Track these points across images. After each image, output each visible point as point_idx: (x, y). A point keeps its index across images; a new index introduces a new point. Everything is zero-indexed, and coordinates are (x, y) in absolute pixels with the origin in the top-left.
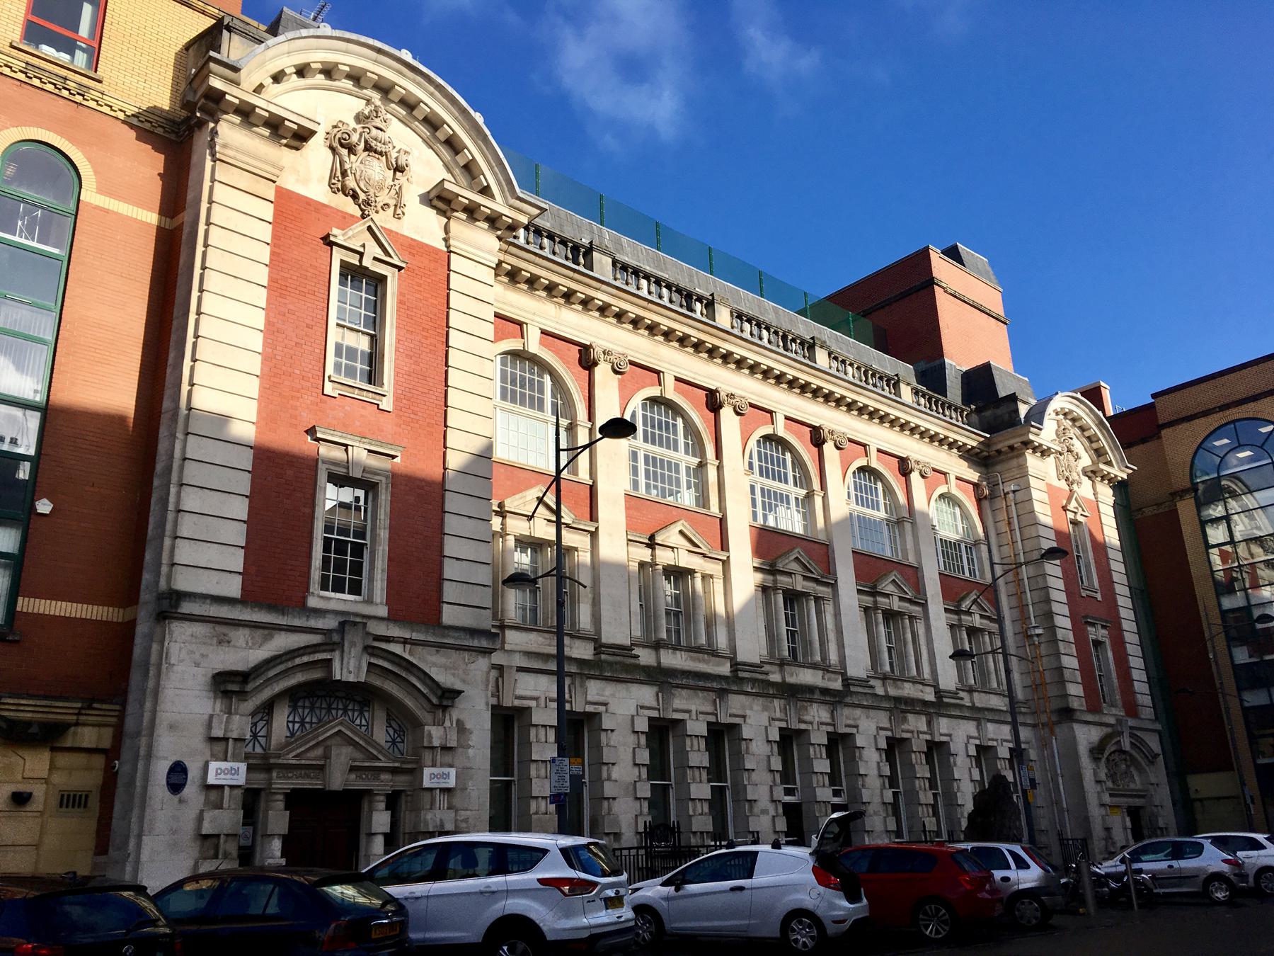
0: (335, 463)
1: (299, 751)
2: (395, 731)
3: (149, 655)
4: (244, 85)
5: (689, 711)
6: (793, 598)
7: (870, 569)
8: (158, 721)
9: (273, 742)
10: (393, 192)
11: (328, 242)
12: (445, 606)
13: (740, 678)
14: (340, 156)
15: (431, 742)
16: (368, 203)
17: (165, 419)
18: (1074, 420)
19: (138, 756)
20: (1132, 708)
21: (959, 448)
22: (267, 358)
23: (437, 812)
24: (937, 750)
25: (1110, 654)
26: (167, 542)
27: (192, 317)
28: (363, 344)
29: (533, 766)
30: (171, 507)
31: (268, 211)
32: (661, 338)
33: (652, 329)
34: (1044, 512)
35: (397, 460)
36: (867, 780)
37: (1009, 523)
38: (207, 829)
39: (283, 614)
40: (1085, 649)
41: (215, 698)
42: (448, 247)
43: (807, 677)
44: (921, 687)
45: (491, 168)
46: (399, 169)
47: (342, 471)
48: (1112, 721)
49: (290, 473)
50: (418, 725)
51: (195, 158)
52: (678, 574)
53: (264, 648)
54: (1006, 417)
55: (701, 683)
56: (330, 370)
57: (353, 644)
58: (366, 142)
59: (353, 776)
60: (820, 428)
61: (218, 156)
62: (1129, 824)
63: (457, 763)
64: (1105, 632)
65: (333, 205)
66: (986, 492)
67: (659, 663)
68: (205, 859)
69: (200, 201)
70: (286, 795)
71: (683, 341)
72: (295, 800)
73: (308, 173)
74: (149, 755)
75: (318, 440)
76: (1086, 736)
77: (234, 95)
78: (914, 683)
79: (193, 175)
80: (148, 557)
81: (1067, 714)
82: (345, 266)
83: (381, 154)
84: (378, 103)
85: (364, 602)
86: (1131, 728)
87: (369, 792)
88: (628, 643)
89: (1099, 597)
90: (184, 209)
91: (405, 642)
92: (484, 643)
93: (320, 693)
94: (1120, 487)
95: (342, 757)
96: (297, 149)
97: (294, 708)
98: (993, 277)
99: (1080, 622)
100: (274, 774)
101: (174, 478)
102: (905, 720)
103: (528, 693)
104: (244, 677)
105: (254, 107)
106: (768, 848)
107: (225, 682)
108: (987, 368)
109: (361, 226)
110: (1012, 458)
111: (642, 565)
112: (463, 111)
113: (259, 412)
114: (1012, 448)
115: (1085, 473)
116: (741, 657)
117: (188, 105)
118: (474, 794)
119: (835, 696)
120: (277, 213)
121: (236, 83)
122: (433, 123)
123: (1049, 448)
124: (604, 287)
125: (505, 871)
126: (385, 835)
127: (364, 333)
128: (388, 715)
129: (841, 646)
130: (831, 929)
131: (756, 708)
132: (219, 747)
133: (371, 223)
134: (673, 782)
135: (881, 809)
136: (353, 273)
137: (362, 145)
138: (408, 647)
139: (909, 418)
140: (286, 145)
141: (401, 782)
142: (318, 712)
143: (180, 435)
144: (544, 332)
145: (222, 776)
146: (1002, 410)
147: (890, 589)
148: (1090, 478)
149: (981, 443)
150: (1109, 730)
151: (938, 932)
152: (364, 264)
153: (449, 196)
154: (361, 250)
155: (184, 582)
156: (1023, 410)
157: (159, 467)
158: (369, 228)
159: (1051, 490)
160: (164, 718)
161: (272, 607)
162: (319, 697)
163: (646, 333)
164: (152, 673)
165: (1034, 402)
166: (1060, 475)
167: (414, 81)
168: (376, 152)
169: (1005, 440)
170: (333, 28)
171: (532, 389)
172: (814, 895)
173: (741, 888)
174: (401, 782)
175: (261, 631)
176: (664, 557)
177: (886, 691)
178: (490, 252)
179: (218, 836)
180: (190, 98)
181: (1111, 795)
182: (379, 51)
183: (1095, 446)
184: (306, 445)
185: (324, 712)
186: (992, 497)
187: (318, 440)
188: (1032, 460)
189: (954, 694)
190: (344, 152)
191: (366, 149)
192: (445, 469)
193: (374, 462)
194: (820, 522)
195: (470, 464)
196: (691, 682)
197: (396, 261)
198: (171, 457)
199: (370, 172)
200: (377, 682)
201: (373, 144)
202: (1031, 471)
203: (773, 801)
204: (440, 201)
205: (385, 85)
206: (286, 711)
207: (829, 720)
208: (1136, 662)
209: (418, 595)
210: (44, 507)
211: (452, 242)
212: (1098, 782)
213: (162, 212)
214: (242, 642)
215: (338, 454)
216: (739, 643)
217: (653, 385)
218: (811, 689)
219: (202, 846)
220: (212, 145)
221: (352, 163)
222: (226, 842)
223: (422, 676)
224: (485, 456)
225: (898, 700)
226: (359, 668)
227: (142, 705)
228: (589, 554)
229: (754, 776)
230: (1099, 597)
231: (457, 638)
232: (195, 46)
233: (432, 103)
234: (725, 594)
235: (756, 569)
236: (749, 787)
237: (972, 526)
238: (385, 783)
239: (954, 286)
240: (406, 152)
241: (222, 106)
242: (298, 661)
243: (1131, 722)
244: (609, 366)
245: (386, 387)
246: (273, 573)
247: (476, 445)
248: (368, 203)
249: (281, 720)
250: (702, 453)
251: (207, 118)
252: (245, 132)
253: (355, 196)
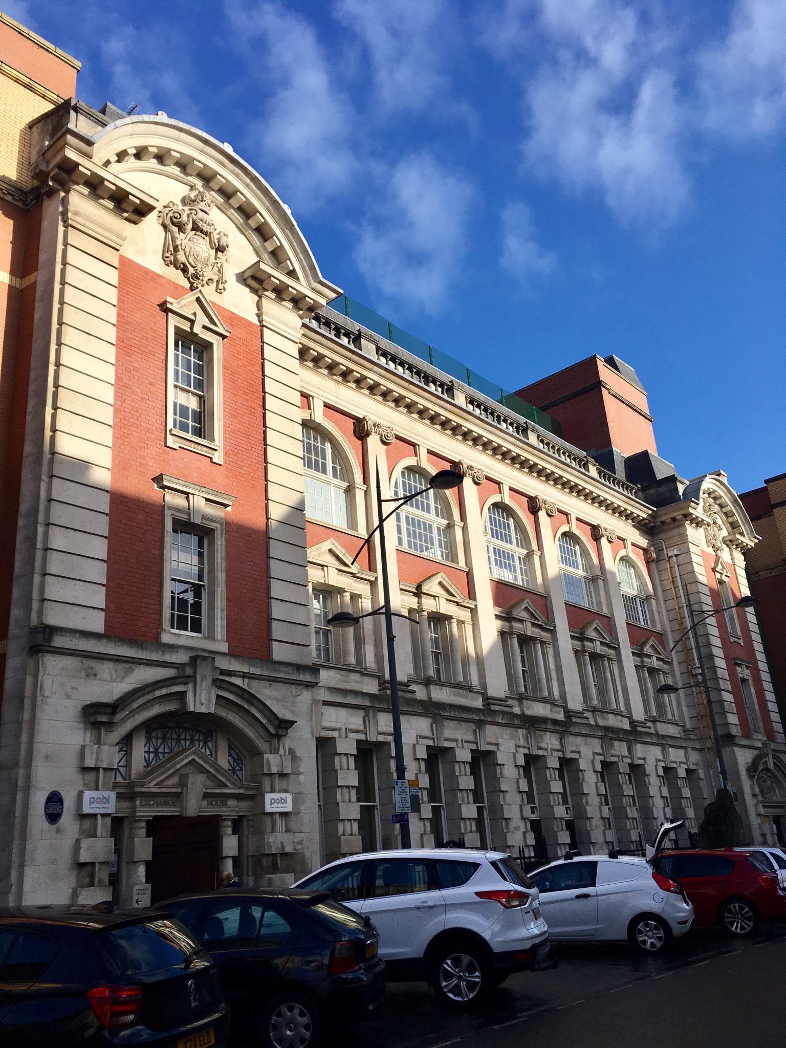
0: (178, 510)
1: (159, 779)
2: (234, 760)
3: (22, 690)
4: (94, 159)
5: (456, 740)
6: (525, 641)
7: (580, 618)
8: (35, 753)
9: (133, 772)
10: (216, 269)
11: (164, 308)
12: (274, 643)
13: (489, 712)
14: (172, 233)
15: (269, 769)
16: (196, 276)
17: (27, 464)
18: (715, 499)
19: (16, 786)
20: (770, 734)
21: (633, 520)
22: (118, 410)
23: (277, 834)
24: (637, 770)
25: (753, 690)
26: (37, 579)
27: (52, 368)
28: (193, 403)
29: (339, 792)
30: (39, 545)
31: (113, 276)
32: (416, 416)
33: (410, 407)
34: (702, 574)
35: (229, 509)
36: (589, 798)
37: (673, 582)
38: (84, 857)
39: (143, 649)
40: (738, 685)
41: (86, 729)
42: (260, 322)
43: (539, 710)
44: (619, 717)
45: (296, 254)
46: (220, 249)
47: (184, 517)
48: (759, 745)
49: (141, 517)
50: (256, 753)
51: (45, 224)
52: (439, 619)
53: (127, 680)
54: (668, 494)
55: (464, 715)
56: (170, 425)
57: (204, 677)
58: (194, 222)
59: (205, 803)
60: (536, 497)
61: (70, 222)
62: (775, 831)
63: (291, 788)
64: (747, 671)
65: (166, 276)
66: (654, 555)
67: (430, 698)
68: (82, 887)
69: (55, 262)
70: (148, 822)
71: (434, 419)
72: (155, 826)
73: (145, 242)
74: (28, 787)
75: (164, 487)
76: (743, 757)
77: (87, 167)
78: (615, 714)
79: (44, 240)
80: (16, 593)
81: (729, 739)
82: (178, 331)
83: (206, 234)
84: (202, 190)
85: (205, 638)
86: (773, 750)
88: (406, 680)
89: (741, 641)
90: (36, 269)
91: (244, 676)
92: (308, 678)
93: (176, 725)
94: (747, 553)
95: (197, 784)
96: (135, 223)
97: (149, 739)
98: (639, 383)
99: (733, 663)
100: (138, 803)
101: (41, 517)
102: (612, 746)
103: (334, 725)
104: (113, 708)
105: (103, 179)
106: (606, 857)
107: (96, 713)
108: (645, 455)
109: (191, 297)
110: (674, 528)
111: (411, 611)
112: (274, 202)
113: (113, 459)
114: (674, 519)
115: (724, 542)
116: (491, 693)
117: (40, 176)
118: (306, 818)
119: (562, 726)
120: (121, 279)
121: (89, 156)
122: (246, 212)
123: (703, 520)
124: (375, 368)
125: (440, 886)
126: (234, 858)
127: (193, 394)
128: (229, 745)
129: (562, 683)
130: (677, 930)
131: (505, 736)
132: (91, 776)
133: (199, 295)
134: (377, 803)
135: (600, 823)
136: (186, 339)
137: (190, 226)
138: (246, 680)
139: (600, 493)
140: (126, 219)
141: (243, 807)
142: (169, 742)
143: (44, 478)
144: (327, 406)
145: (95, 805)
146: (663, 489)
148: (728, 546)
149: (649, 515)
150: (756, 752)
151: (742, 928)
152: (195, 331)
153: (262, 276)
154: (193, 318)
155: (55, 617)
156: (681, 488)
157: (24, 507)
158: (198, 300)
159: (704, 554)
160: (40, 749)
161: (133, 642)
162: (169, 728)
163: (405, 410)
164: (27, 704)
165: (688, 483)
166: (708, 542)
167: (233, 172)
168: (202, 231)
169: (667, 514)
170: (169, 116)
171: (316, 455)
172: (658, 899)
173: (587, 896)
174: (243, 807)
175: (124, 665)
176: (429, 605)
177: (596, 721)
178: (294, 329)
179: (93, 864)
180: (43, 167)
181: (764, 807)
182: (206, 142)
183: (730, 520)
184: (153, 493)
185: (174, 742)
186: (658, 561)
187: (164, 487)
188: (691, 531)
189: (643, 724)
190: (175, 229)
191: (193, 229)
192: (268, 519)
193: (211, 510)
194: (539, 579)
195: (289, 516)
196: (457, 714)
197: (220, 330)
198: (37, 497)
199: (198, 249)
200: (223, 713)
201: (200, 224)
202: (690, 539)
203: (523, 818)
204: (254, 280)
205: (207, 174)
206: (143, 741)
207: (559, 747)
208: (770, 696)
209: (253, 631)
211: (264, 317)
212: (754, 795)
213: (13, 272)
214: (106, 675)
215: (180, 501)
216: (489, 681)
217: (410, 456)
218: (545, 720)
219: (78, 874)
220: (64, 214)
221: (181, 238)
222: (100, 869)
223: (261, 707)
224: (299, 509)
225: (607, 729)
226: (209, 700)
227: (18, 736)
228: (369, 601)
229: (508, 795)
230: (741, 641)
231: (286, 673)
232: (40, 125)
233: (248, 194)
234: (474, 638)
235: (497, 617)
236: (505, 807)
237: (643, 585)
238: (232, 809)
239: (615, 389)
240: (225, 235)
241: (74, 177)
242: (158, 693)
243: (773, 746)
244: (378, 438)
245: (217, 442)
246: (133, 607)
247: (292, 499)
248: (196, 276)
249: (139, 749)
250: (449, 516)
251: (59, 187)
252: (92, 203)
253: (184, 270)
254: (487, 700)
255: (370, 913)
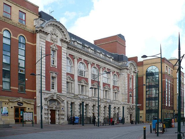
31: (45, 44)
87: (56, 110)
93: (52, 100)
144: (69, 54)
147: (83, 82)
210: (26, 79)
254: (89, 97)
255: (130, 126)
